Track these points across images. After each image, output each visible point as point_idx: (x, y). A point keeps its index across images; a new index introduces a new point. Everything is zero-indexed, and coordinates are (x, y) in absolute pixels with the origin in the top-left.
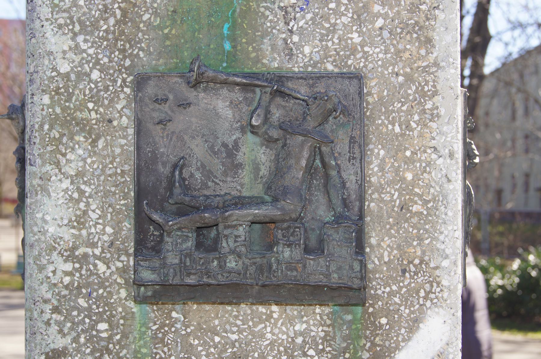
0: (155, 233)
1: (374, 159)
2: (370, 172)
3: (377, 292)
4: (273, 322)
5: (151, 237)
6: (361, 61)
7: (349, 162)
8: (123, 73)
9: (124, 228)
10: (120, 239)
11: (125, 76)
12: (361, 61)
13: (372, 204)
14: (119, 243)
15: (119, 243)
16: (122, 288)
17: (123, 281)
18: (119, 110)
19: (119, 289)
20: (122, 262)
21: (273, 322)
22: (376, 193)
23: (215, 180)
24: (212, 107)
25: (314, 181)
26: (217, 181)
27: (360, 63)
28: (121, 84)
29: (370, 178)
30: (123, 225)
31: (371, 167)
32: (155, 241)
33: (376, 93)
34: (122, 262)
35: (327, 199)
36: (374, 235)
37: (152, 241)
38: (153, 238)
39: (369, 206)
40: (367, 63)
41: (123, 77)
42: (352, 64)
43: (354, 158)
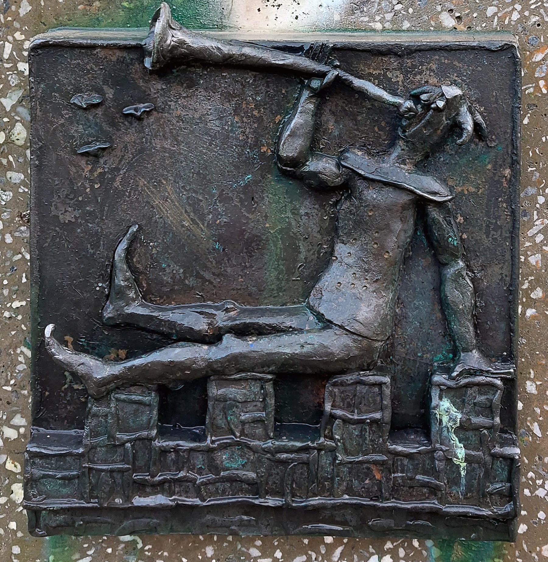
0: (76, 387)
1: (536, 217)
2: (528, 244)
3: (537, 492)
4: (323, 552)
5: (66, 395)
6: (514, 9)
7: (488, 237)
8: (16, 30)
9: (21, 359)
10: (12, 382)
11: (18, 36)
12: (514, 9)
13: (530, 312)
14: (9, 389)
15: (9, 389)
16: (17, 481)
17: (19, 466)
18: (8, 109)
19: (10, 484)
20: (17, 428)
21: (323, 552)
22: (538, 289)
23: (202, 273)
24: (197, 116)
25: (413, 276)
26: (207, 275)
27: (511, 12)
28: (11, 53)
29: (527, 256)
30: (18, 351)
31: (530, 233)
32: (76, 403)
33: (542, 78)
34: (17, 428)
35: (439, 315)
36: (532, 376)
37: (69, 403)
38: (72, 397)
39: (524, 313)
40: (527, 13)
41: (15, 39)
42: (496, 14)
43: (497, 228)
